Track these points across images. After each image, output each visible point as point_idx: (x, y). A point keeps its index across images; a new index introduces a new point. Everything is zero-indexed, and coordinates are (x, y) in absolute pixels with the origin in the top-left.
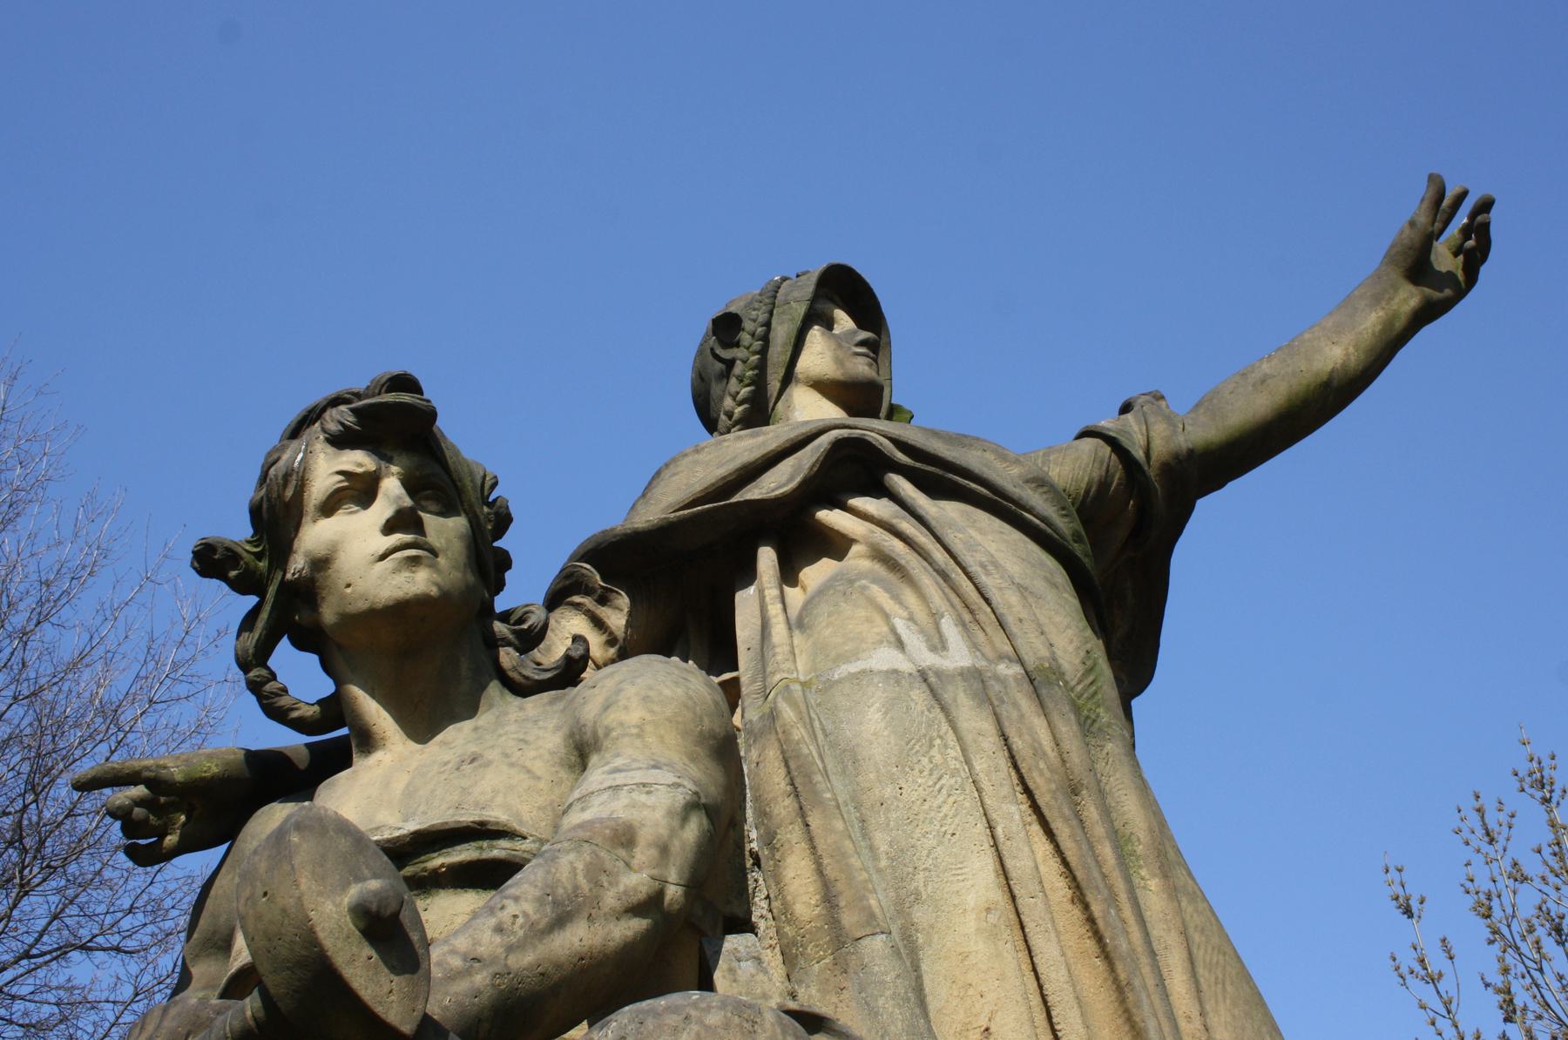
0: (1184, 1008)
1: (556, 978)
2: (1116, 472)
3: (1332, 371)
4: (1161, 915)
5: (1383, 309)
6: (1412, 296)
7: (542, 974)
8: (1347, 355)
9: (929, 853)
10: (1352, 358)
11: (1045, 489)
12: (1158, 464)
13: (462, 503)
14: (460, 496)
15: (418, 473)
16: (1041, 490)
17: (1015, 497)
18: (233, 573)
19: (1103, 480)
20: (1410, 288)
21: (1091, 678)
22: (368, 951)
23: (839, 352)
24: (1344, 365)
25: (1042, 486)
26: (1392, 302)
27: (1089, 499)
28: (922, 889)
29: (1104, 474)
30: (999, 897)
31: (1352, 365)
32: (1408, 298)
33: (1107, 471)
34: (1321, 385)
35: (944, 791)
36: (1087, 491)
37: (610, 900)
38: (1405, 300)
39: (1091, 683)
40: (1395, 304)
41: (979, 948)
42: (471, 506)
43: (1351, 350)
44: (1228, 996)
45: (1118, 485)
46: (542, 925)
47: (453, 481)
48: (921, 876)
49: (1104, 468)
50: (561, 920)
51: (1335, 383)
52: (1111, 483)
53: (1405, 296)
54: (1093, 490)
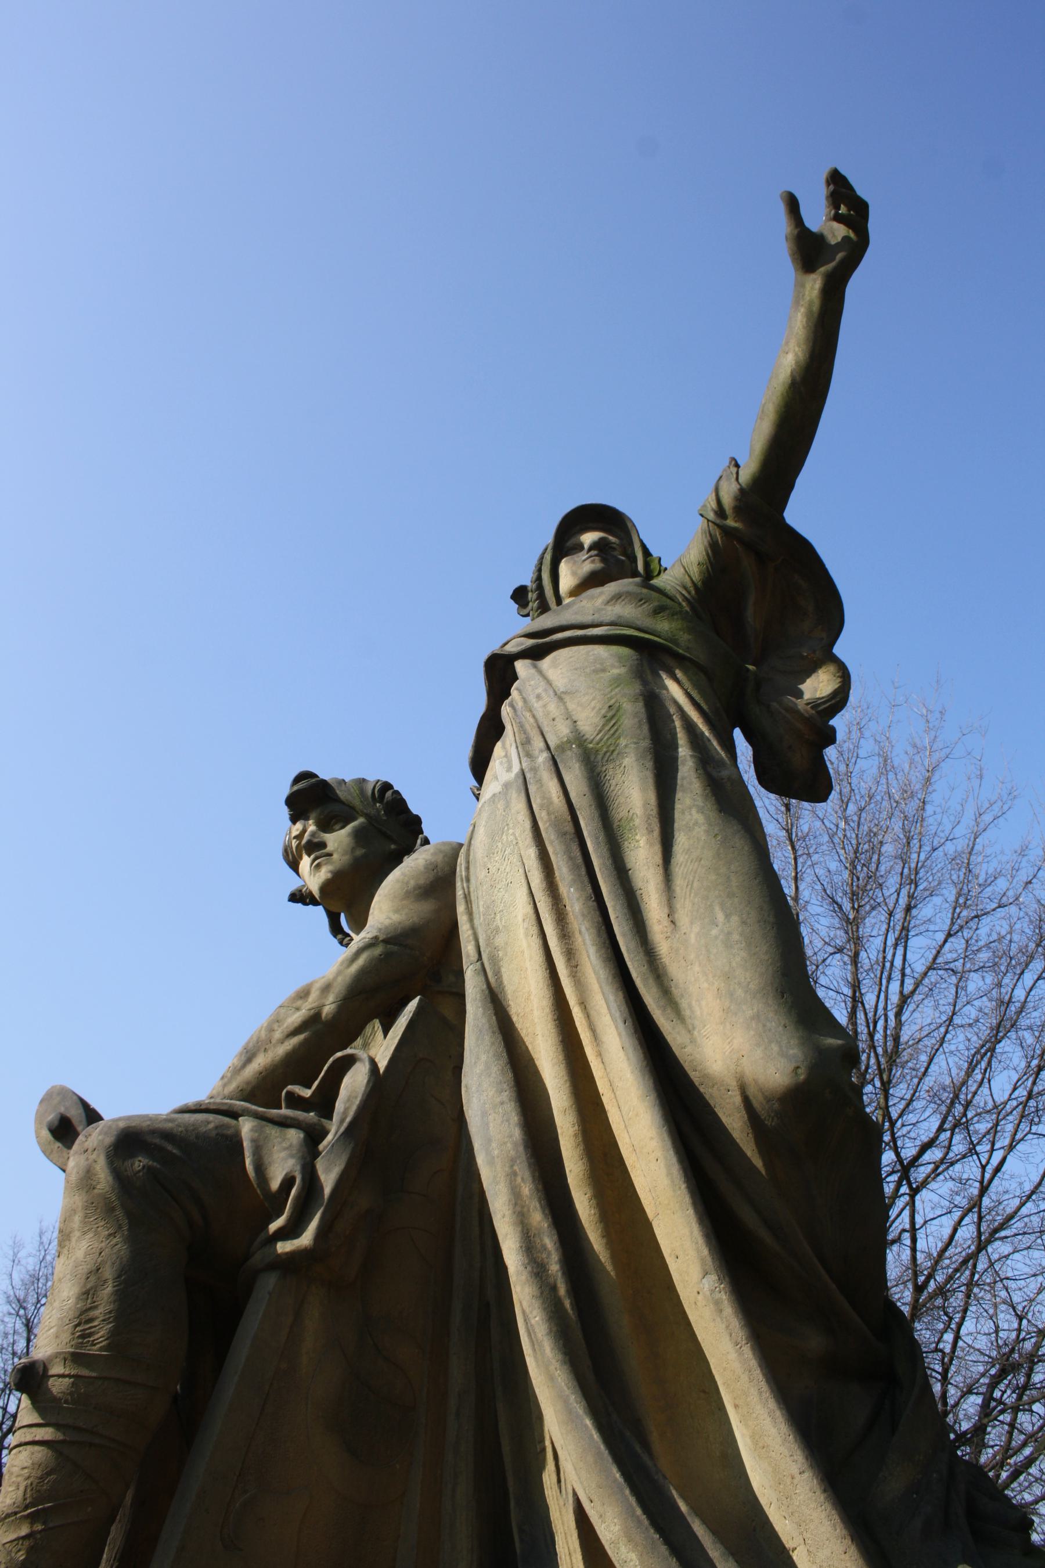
0: (657, 917)
1: (249, 1089)
2: (715, 532)
3: (792, 373)
4: (645, 861)
5: (802, 305)
6: (815, 281)
7: (241, 1090)
8: (796, 355)
9: (502, 900)
10: (800, 354)
11: (623, 598)
12: (731, 511)
13: (357, 812)
14: (355, 810)
15: (322, 817)
16: (620, 600)
17: (590, 623)
18: (308, 900)
19: (711, 542)
20: (813, 276)
21: (613, 722)
22: (58, 1144)
23: (574, 568)
24: (797, 363)
25: (620, 597)
26: (805, 297)
27: (712, 559)
28: (499, 924)
29: (709, 538)
30: (529, 909)
31: (802, 358)
32: (812, 285)
33: (711, 535)
34: (790, 388)
35: (506, 859)
36: (708, 554)
37: (278, 1035)
38: (812, 288)
39: (613, 726)
40: (807, 298)
41: (524, 944)
42: (362, 811)
43: (797, 349)
44: (693, 891)
45: (722, 538)
46: (238, 1068)
47: (348, 806)
48: (498, 917)
49: (708, 535)
50: (249, 1060)
51: (798, 379)
52: (717, 541)
53: (811, 285)
54: (709, 551)
